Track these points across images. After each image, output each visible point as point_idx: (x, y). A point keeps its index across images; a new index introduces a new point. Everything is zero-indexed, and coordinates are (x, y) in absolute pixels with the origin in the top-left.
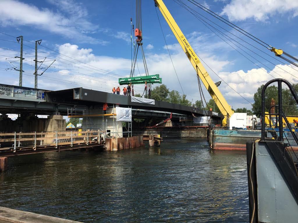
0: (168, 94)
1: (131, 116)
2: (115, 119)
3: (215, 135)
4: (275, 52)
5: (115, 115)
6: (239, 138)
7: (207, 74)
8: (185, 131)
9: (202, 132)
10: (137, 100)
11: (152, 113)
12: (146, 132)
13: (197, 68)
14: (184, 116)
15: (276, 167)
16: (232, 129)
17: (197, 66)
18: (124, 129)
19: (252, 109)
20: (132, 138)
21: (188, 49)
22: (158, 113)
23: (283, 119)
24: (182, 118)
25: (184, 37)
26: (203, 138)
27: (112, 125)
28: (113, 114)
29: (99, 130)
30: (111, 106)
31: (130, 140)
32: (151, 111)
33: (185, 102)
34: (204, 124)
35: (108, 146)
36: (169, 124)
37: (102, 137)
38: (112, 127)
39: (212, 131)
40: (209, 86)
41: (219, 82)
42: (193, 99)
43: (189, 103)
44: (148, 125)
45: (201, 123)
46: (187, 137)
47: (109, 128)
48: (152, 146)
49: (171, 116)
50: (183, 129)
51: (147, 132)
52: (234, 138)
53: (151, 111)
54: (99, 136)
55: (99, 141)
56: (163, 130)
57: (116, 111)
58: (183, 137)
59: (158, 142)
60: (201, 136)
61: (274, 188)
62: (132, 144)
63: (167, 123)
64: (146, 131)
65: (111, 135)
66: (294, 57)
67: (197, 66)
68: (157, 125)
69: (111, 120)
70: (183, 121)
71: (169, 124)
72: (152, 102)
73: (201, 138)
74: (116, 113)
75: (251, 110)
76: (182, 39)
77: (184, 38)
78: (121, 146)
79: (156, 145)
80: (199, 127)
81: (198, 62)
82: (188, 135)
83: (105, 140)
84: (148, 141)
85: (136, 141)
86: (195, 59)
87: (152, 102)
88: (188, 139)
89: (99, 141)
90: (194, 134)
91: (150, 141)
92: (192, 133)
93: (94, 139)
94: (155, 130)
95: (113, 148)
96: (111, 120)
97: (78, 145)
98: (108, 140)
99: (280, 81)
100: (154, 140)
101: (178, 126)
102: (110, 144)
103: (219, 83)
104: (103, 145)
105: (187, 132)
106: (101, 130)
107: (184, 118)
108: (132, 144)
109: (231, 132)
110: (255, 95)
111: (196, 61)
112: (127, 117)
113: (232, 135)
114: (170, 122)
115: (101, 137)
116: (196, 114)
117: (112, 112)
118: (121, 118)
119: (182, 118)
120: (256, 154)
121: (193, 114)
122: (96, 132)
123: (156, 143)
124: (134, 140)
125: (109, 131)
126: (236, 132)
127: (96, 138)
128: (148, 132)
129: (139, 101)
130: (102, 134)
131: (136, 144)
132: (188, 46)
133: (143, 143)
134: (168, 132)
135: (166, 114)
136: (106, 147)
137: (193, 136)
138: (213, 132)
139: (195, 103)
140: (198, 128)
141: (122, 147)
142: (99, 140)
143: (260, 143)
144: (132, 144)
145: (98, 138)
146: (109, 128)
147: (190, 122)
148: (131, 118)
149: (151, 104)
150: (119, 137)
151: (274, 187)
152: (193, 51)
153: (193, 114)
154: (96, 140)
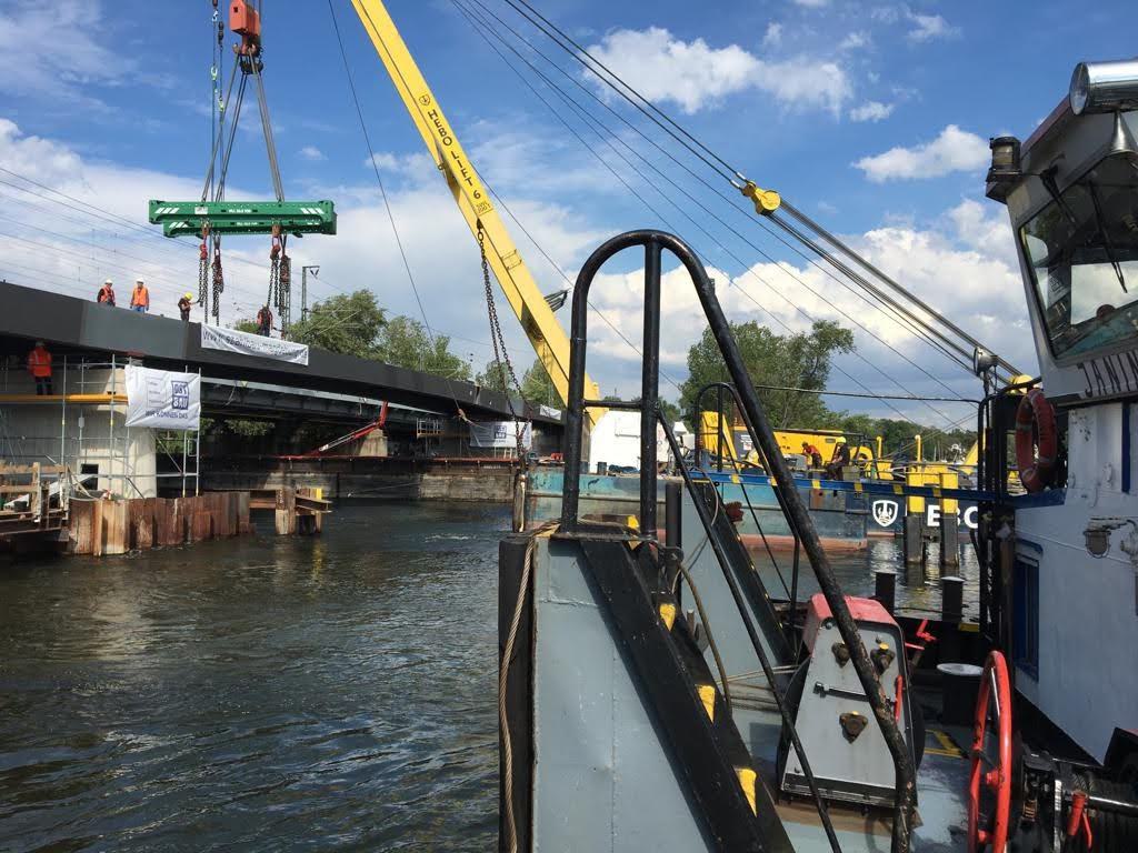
0: (381, 329)
1: (196, 406)
2: (120, 418)
3: (534, 492)
4: (756, 200)
5: (123, 401)
6: (621, 504)
7: (515, 259)
8: (434, 475)
9: (497, 480)
10: (228, 340)
11: (303, 399)
12: (277, 475)
13: (482, 230)
14: (435, 417)
15: (619, 662)
16: (596, 472)
17: (480, 225)
18: (163, 463)
19: (680, 401)
20: (198, 501)
21: (447, 151)
22: (328, 402)
23: (660, 427)
24: (426, 424)
25: (433, 99)
26: (500, 502)
27: (105, 444)
28: (111, 397)
29: (36, 465)
30: (104, 359)
31: (186, 511)
32: (302, 392)
33: (444, 362)
34: (508, 449)
35: (80, 536)
36: (376, 446)
37: (51, 493)
38: (106, 452)
39: (523, 476)
40: (524, 303)
41: (562, 292)
42: (475, 361)
43: (460, 369)
44: (289, 449)
45: (496, 445)
46: (443, 499)
47: (95, 458)
48: (289, 535)
49: (382, 414)
50: (426, 466)
51: (280, 474)
52: (603, 504)
53: (302, 392)
54: (39, 490)
55: (39, 513)
56: (344, 469)
57: (123, 383)
58: (424, 500)
59: (314, 517)
60: (494, 495)
61: (607, 769)
62: (199, 525)
63: (365, 443)
64: (276, 469)
65: (102, 485)
66: (834, 236)
67: (480, 225)
68: (325, 447)
69: (100, 422)
70: (428, 438)
71: (376, 446)
72: (295, 354)
73: (491, 501)
74: (123, 389)
75: (678, 406)
76: (426, 110)
77: (434, 105)
78: (144, 534)
79: (304, 528)
80: (488, 459)
81: (483, 207)
82: (445, 491)
83: (66, 508)
84: (273, 511)
85: (217, 511)
86: (475, 196)
87: (299, 354)
88: (445, 506)
89: (37, 510)
90: (467, 487)
91: (280, 513)
92: (460, 484)
93: (11, 504)
94: (317, 470)
95: (104, 542)
96: (100, 422)
97: (16, 523)
98: (83, 506)
99: (653, 240)
100: (296, 509)
101: (410, 455)
102: (93, 524)
103: (562, 296)
104: (59, 531)
105: (440, 478)
106: (53, 465)
107: (436, 423)
108: (198, 528)
109: (593, 482)
110: (694, 353)
111: (476, 202)
112: (175, 411)
113: (595, 492)
114: (377, 440)
115: (45, 492)
116: (473, 411)
117: (109, 388)
118: (148, 414)
119: (426, 424)
120: (536, 599)
121: (461, 411)
122: (21, 470)
123: (305, 521)
124: (207, 507)
125: (92, 469)
126: (610, 480)
127: (25, 498)
128: (284, 478)
129: (237, 344)
130: (53, 480)
131: (216, 523)
132: (448, 141)
133: (247, 523)
134: (369, 476)
135: (365, 405)
136: (71, 539)
137: (463, 493)
138: (529, 481)
139: (484, 372)
140: (483, 463)
141: (149, 538)
142: (39, 506)
143: (557, 545)
144: (198, 528)
145: (31, 501)
146: (91, 455)
147: (458, 438)
148: (195, 416)
149: (293, 361)
150: (137, 496)
151: (610, 766)
152: (466, 164)
153: (461, 411)
154: (22, 507)
